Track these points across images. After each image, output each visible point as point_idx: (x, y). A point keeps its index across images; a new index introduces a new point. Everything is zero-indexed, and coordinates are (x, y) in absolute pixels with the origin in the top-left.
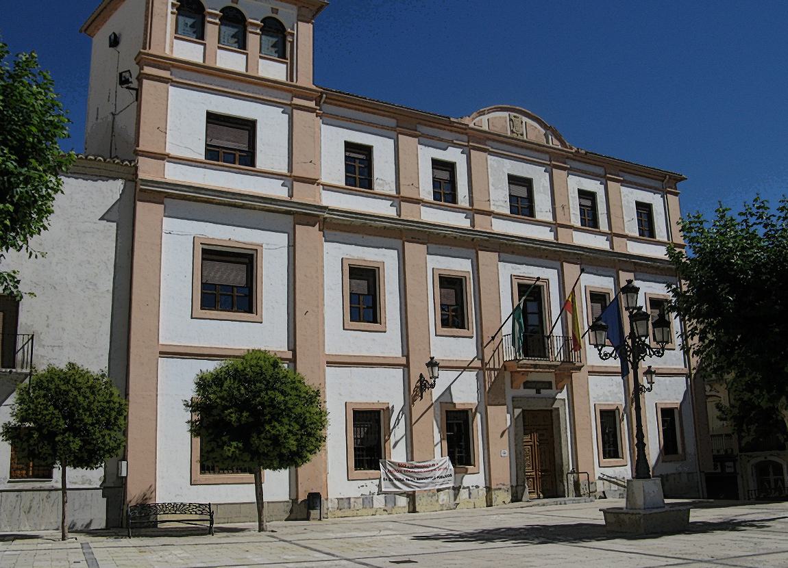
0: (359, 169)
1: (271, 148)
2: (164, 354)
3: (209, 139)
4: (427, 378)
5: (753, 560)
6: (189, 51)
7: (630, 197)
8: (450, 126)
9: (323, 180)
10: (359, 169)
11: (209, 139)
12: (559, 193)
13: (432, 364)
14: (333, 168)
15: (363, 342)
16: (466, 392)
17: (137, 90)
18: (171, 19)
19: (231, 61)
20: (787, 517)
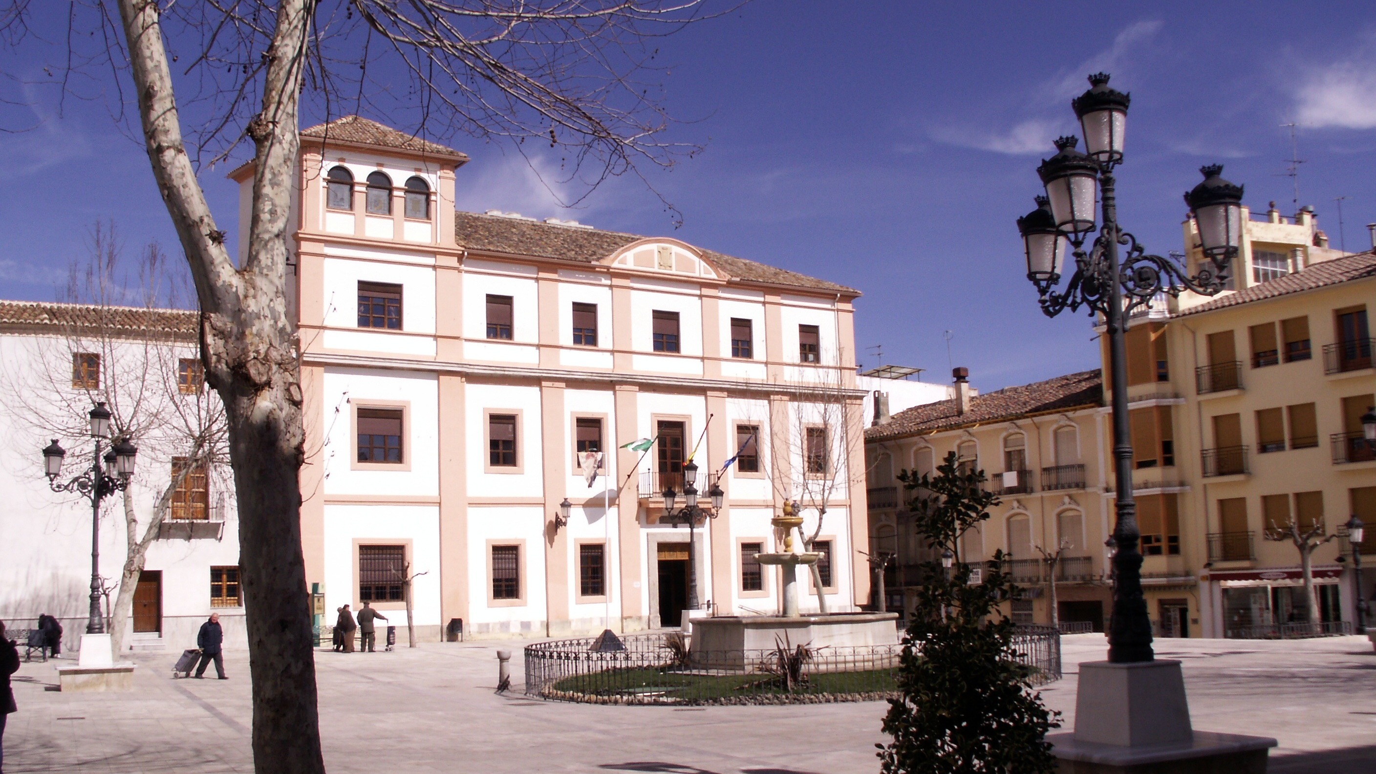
0: (500, 320)
1: (416, 309)
2: (327, 501)
3: (752, 441)
4: (561, 517)
5: (497, 246)
6: (339, 224)
7: (794, 315)
8: (590, 270)
9: (466, 335)
10: (500, 320)
11: (752, 441)
12: (705, 322)
13: (566, 505)
14: (476, 320)
15: (503, 482)
16: (604, 530)
17: (295, 265)
18: (322, 194)
19: (379, 228)
20: (158, 23)
